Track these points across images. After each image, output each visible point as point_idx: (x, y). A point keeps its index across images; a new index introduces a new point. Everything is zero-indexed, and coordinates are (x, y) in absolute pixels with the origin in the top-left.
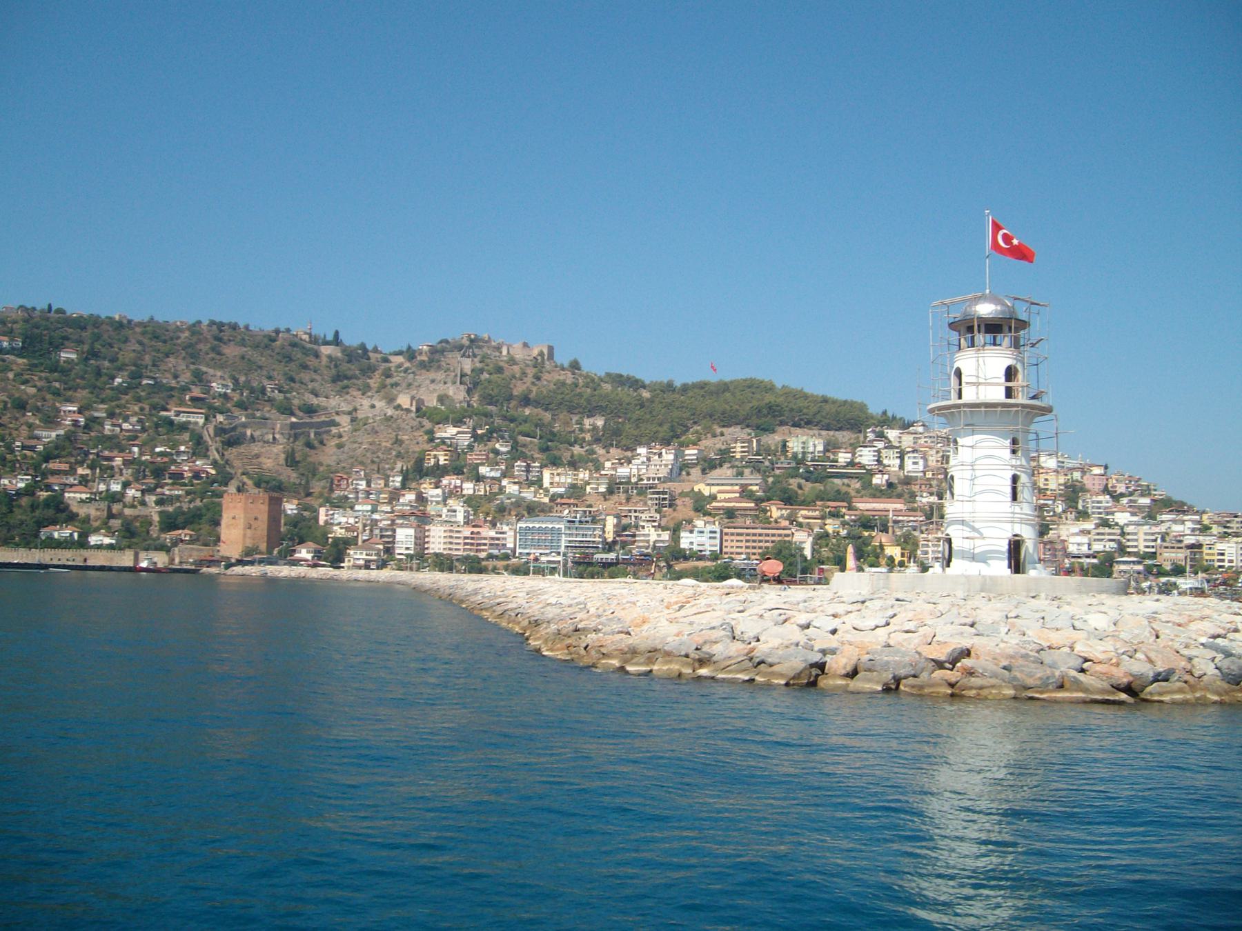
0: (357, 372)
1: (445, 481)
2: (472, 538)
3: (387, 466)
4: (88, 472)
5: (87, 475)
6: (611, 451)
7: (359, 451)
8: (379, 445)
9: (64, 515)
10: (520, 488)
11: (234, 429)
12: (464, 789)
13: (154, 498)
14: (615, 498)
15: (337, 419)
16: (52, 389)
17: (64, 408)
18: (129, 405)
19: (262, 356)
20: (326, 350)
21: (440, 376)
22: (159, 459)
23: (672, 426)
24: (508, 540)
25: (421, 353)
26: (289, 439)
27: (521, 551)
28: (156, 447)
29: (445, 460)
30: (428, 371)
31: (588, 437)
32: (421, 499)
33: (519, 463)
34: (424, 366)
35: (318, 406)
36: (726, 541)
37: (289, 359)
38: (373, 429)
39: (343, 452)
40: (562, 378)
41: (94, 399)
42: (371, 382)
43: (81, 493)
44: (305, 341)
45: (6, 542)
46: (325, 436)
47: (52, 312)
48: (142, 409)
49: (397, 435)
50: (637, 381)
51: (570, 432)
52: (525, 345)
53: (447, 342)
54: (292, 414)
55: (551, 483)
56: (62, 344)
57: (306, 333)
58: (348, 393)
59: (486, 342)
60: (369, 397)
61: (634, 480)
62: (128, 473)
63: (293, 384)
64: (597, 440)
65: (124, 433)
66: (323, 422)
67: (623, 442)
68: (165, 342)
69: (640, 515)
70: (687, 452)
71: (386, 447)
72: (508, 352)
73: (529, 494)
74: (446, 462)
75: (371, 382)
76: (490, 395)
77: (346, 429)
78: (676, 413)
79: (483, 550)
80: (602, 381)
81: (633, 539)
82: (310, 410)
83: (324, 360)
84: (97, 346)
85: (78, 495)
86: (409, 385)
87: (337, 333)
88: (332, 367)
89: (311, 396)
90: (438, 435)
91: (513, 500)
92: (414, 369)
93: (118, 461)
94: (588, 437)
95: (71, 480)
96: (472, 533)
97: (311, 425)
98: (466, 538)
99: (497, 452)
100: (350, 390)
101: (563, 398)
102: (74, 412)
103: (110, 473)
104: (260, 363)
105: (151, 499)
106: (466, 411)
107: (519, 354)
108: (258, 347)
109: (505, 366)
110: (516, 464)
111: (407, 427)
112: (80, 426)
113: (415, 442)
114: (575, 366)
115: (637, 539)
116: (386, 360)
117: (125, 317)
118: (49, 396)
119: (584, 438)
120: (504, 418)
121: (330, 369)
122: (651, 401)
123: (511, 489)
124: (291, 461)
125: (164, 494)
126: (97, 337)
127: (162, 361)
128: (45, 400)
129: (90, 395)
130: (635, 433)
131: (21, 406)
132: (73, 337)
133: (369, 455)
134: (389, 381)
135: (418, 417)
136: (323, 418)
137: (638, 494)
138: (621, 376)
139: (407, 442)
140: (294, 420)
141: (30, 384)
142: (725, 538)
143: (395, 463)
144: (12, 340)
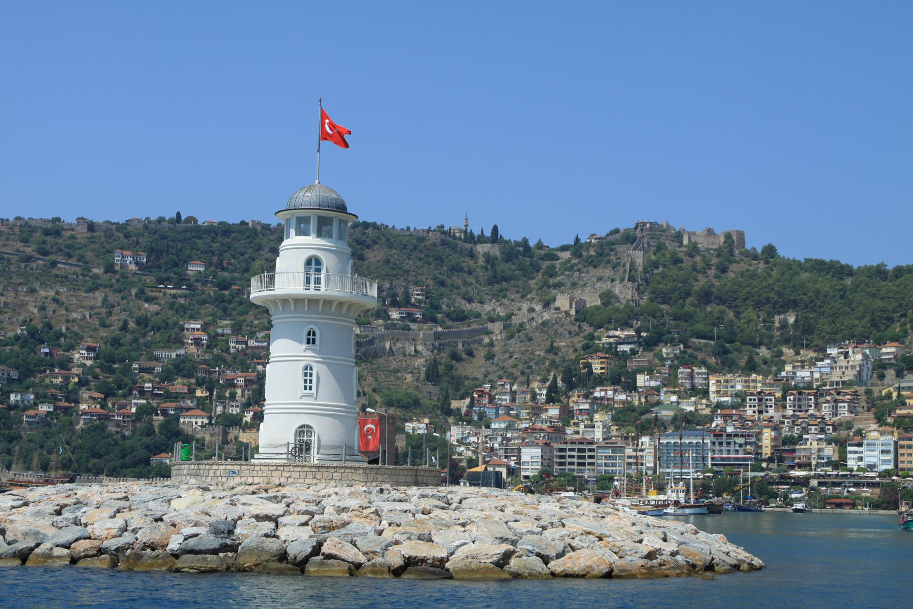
6: (802, 352)
8: (532, 353)
11: (371, 342)
15: (490, 326)
19: (409, 259)
20: (481, 249)
23: (873, 320)
26: (432, 351)
29: (602, 368)
30: (595, 267)
34: (593, 263)
36: (903, 455)
39: (493, 364)
42: (532, 283)
45: (908, 416)
46: (474, 347)
49: (552, 342)
58: (504, 297)
59: (664, 231)
64: (787, 341)
70: (884, 350)
71: (539, 355)
74: (603, 371)
78: (879, 303)
82: (461, 317)
83: (481, 261)
87: (495, 229)
88: (489, 266)
89: (463, 302)
92: (580, 266)
97: (459, 334)
100: (508, 293)
102: (198, 330)
104: (406, 267)
110: (679, 371)
114: (770, 251)
117: (259, 223)
124: (433, 375)
134: (552, 281)
139: (563, 350)
142: (901, 451)
143: (549, 371)
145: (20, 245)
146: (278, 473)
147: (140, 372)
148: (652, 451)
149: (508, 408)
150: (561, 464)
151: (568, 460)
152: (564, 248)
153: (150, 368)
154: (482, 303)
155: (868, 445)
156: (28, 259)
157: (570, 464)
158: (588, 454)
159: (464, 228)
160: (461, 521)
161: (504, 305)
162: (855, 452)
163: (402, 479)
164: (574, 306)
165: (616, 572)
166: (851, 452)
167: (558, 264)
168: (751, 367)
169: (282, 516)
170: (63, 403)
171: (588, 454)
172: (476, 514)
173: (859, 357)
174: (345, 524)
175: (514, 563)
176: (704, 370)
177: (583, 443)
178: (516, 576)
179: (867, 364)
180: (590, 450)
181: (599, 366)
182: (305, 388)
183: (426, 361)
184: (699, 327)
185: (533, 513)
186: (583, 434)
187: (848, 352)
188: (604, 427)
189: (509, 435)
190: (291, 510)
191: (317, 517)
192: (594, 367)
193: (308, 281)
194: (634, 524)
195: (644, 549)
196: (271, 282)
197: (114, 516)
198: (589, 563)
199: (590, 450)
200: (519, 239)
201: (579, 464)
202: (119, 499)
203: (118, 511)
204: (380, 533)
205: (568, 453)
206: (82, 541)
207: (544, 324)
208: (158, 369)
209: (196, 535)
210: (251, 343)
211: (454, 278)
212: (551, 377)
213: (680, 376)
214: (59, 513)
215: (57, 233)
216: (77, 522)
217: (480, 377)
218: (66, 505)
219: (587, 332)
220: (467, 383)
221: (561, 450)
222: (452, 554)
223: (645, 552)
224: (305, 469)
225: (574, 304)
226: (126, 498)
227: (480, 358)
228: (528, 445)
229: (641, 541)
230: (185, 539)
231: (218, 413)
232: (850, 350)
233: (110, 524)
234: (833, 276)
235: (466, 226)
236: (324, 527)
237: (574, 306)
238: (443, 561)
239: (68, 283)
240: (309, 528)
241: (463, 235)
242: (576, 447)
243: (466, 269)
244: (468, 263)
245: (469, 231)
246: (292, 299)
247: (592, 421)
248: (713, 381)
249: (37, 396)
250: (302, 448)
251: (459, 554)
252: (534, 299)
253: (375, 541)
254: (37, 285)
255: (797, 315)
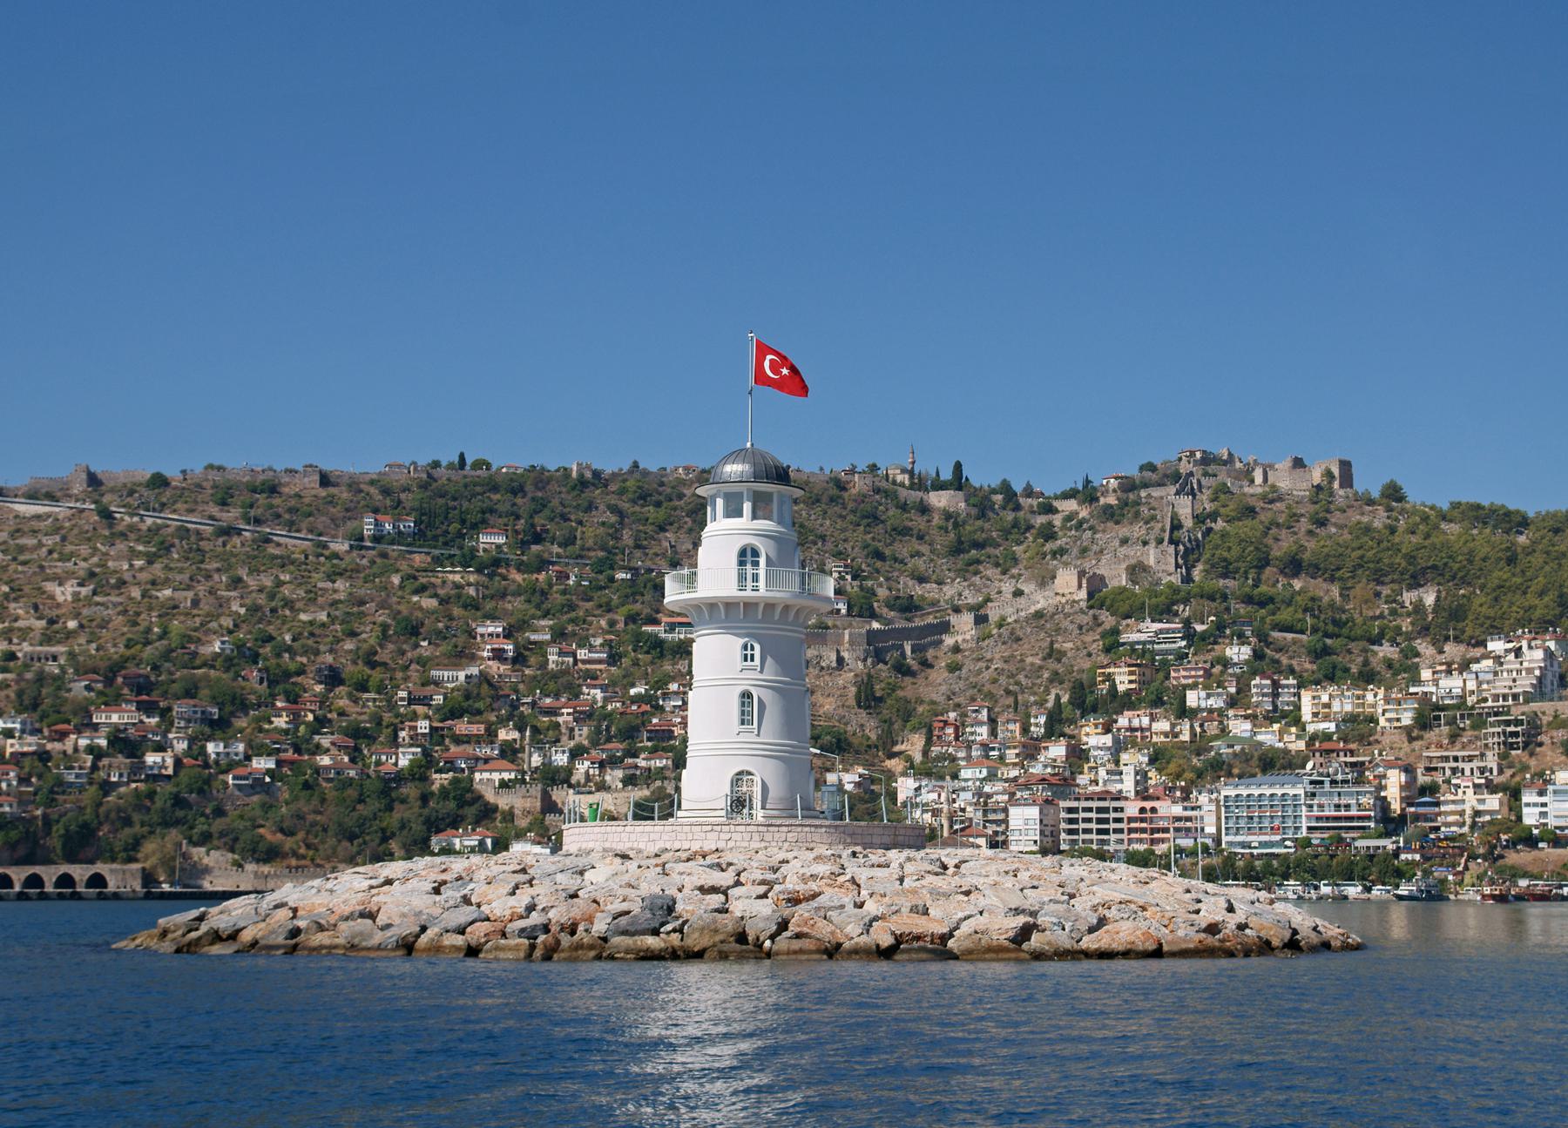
0: (994, 534)
1: (1123, 721)
2: (1142, 820)
3: (1032, 699)
4: (516, 735)
5: (515, 740)
6: (1446, 648)
7: (986, 675)
8: (1022, 661)
9: (470, 811)
10: (1255, 725)
12: (569, 1076)
13: (619, 773)
14: (1431, 735)
16: (464, 598)
17: (480, 630)
18: (590, 618)
21: (1138, 530)
22: (634, 707)
24: (1206, 820)
25: (1105, 493)
27: (1231, 838)
28: (633, 685)
29: (1131, 682)
30: (1117, 523)
31: (1406, 625)
32: (1078, 755)
33: (1257, 681)
34: (1110, 514)
35: (923, 598)
37: (873, 518)
38: (1012, 634)
40: (1365, 519)
41: (533, 611)
43: (500, 771)
44: (902, 485)
46: (930, 653)
47: (468, 468)
48: (612, 623)
49: (1052, 643)
50: (1508, 514)
51: (1375, 618)
52: (1298, 463)
53: (1151, 467)
54: (873, 615)
55: (1315, 715)
56: (484, 521)
57: (904, 471)
58: (976, 573)
59: (1225, 463)
60: (1013, 577)
61: (1471, 700)
62: (583, 734)
63: (879, 564)
64: (1424, 631)
65: (580, 665)
66: (929, 625)
67: (1469, 631)
68: (658, 504)
69: (1461, 765)
71: (1032, 664)
72: (1265, 479)
73: (1268, 737)
74: (1133, 686)
75: (1018, 549)
76: (1225, 560)
77: (968, 637)
79: (1163, 841)
80: (1444, 518)
81: (1437, 809)
82: (909, 607)
84: (539, 520)
85: (496, 776)
86: (1084, 551)
87: (958, 467)
90: (1124, 638)
91: (1238, 748)
93: (565, 718)
94: (1406, 625)
95: (486, 751)
96: (1142, 810)
97: (905, 634)
98: (1130, 820)
99: (1226, 663)
101: (1362, 557)
102: (498, 636)
103: (544, 737)
104: (820, 530)
105: (614, 776)
106: (1176, 590)
107: (1284, 480)
108: (818, 501)
109: (1259, 505)
110: (1253, 683)
111: (1071, 627)
112: (506, 659)
113: (1080, 650)
114: (1393, 493)
115: (1443, 808)
116: (1049, 509)
117: (588, 467)
118: (457, 611)
119: (1399, 628)
120: (1248, 600)
121: (947, 532)
122: (1529, 551)
123: (1240, 727)
124: (868, 699)
125: (636, 767)
126: (541, 505)
127: (652, 538)
128: (451, 619)
129: (526, 606)
130: (1491, 613)
131: (413, 630)
132: (501, 508)
133: (1003, 680)
134: (1049, 546)
135: (1091, 607)
136: (930, 620)
137: (1474, 727)
138: (1478, 507)
140: (876, 625)
141: (427, 593)
143: (1047, 691)
144: (396, 521)
145: (214, 510)
146: (713, 835)
147: (409, 704)
148: (1214, 808)
149: (985, 747)
150: (1070, 832)
151: (1083, 826)
152: (1067, 495)
153: (425, 697)
154: (940, 583)
155: (1555, 792)
156: (228, 532)
157: (1086, 831)
158: (1113, 815)
159: (909, 467)
160: (963, 889)
161: (974, 585)
162: (1535, 805)
163: (876, 840)
164: (1084, 585)
165: (1165, 948)
166: (1528, 805)
167: (1057, 520)
168: (1367, 677)
169: (733, 887)
170: (290, 754)
171: (1113, 815)
172: (982, 880)
173: (1539, 654)
174: (815, 896)
175: (1036, 941)
176: (1292, 681)
177: (1105, 799)
178: (1038, 956)
179: (1552, 666)
180: (1116, 810)
181: (1126, 678)
182: (743, 723)
183: (856, 675)
184: (1285, 615)
185: (1056, 879)
186: (1105, 782)
187: (1521, 648)
188: (1137, 773)
189: (987, 789)
190: (742, 879)
191: (777, 888)
192: (1118, 679)
193: (742, 578)
194: (1188, 891)
195: (1205, 918)
196: (692, 580)
197: (513, 893)
198: (1132, 938)
199: (1116, 810)
200: (995, 483)
201: (1099, 832)
202: (514, 872)
203: (517, 887)
204: (860, 905)
205: (1083, 815)
206: (478, 924)
207: (1039, 615)
208: (438, 699)
209: (628, 913)
210: (582, 654)
211: (897, 545)
212: (1052, 698)
213: (1254, 690)
214: (437, 891)
215: (272, 489)
216: (466, 900)
217: (940, 699)
218: (444, 882)
219: (1107, 626)
220: (920, 709)
221: (1070, 810)
222: (957, 928)
223: (1204, 925)
224: (750, 828)
225: (1084, 582)
226: (524, 871)
227: (939, 675)
228: (1017, 803)
229: (1197, 912)
230: (614, 918)
231: (534, 764)
232: (1524, 644)
233: (512, 901)
234: (1495, 527)
235: (913, 463)
236: (789, 900)
237: (1084, 585)
238: (945, 938)
239: (292, 567)
240: (769, 901)
241: (907, 476)
242: (1094, 804)
243: (915, 532)
244: (918, 522)
245: (916, 472)
246: (704, 604)
247: (1117, 762)
248: (1306, 698)
249: (249, 745)
250: (739, 804)
251: (966, 928)
252: (1020, 575)
253: (856, 915)
254: (243, 572)
255: (1439, 591)
